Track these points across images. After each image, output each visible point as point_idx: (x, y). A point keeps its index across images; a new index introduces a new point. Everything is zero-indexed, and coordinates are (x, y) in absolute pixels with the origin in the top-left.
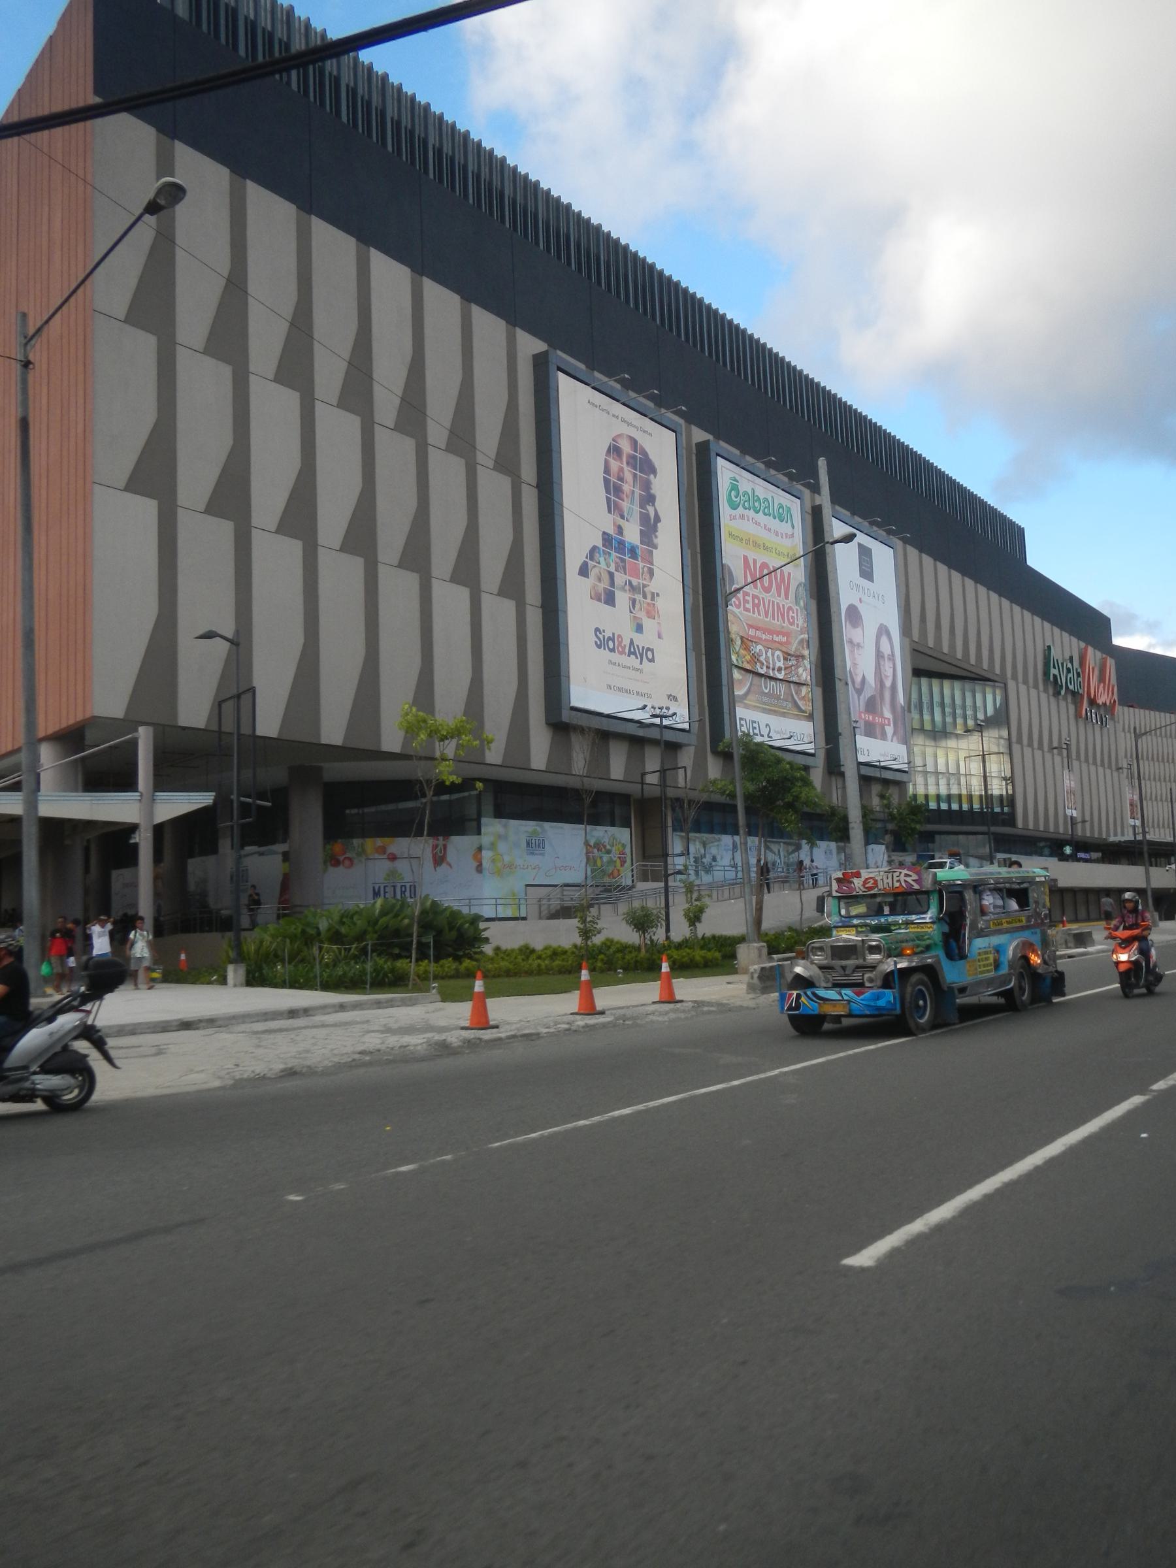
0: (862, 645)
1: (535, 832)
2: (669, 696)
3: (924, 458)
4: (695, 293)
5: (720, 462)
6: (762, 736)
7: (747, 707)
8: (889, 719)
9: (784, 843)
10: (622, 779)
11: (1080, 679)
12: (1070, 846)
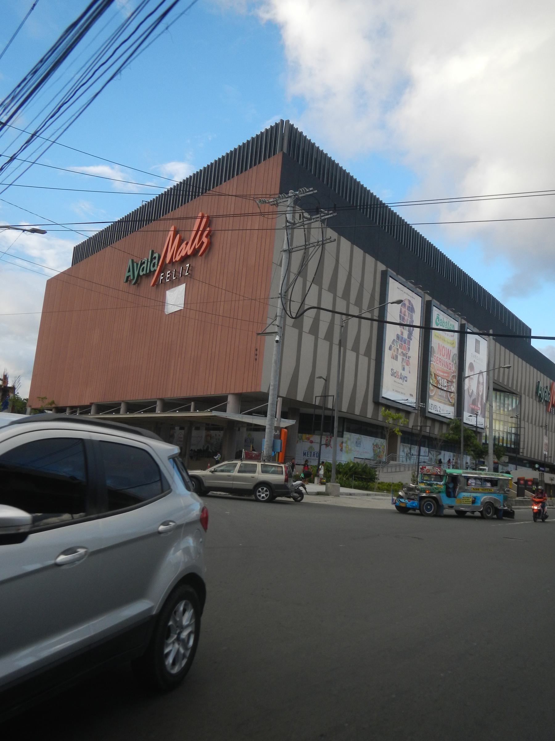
0: (473, 378)
1: (359, 439)
2: (410, 394)
3: (428, 241)
4: (373, 193)
5: (434, 308)
6: (438, 411)
7: (434, 400)
8: (479, 408)
9: (435, 451)
10: (381, 421)
11: (550, 396)
12: (538, 464)
